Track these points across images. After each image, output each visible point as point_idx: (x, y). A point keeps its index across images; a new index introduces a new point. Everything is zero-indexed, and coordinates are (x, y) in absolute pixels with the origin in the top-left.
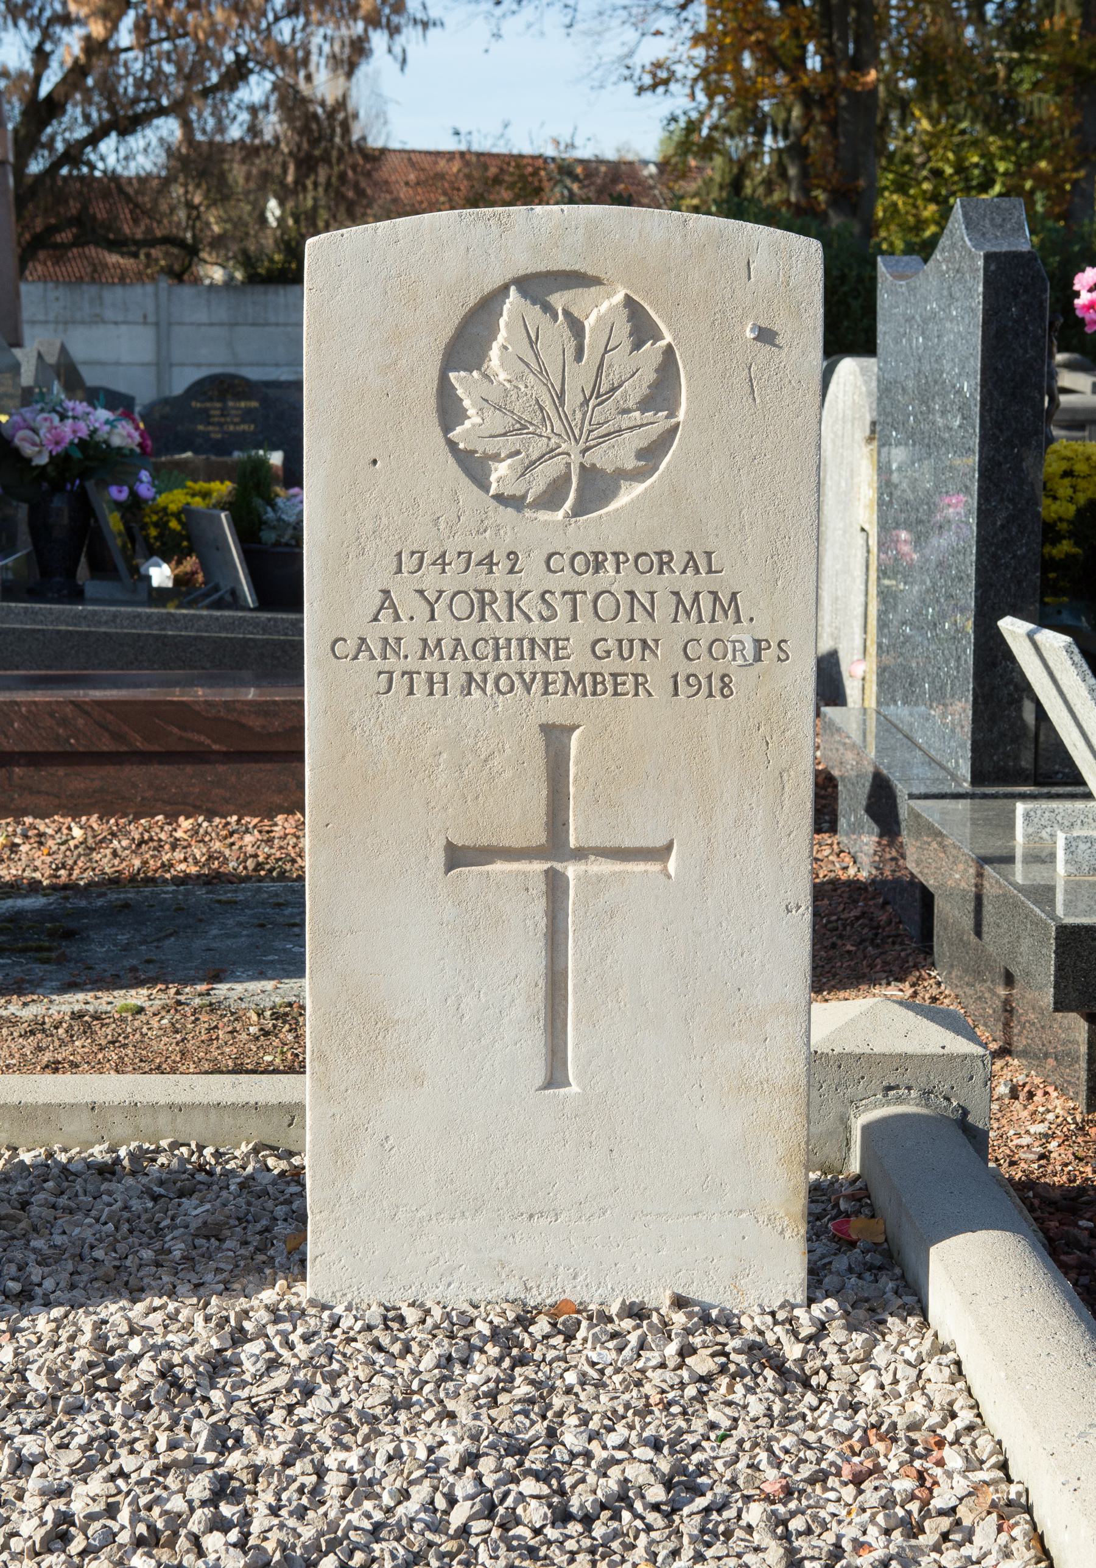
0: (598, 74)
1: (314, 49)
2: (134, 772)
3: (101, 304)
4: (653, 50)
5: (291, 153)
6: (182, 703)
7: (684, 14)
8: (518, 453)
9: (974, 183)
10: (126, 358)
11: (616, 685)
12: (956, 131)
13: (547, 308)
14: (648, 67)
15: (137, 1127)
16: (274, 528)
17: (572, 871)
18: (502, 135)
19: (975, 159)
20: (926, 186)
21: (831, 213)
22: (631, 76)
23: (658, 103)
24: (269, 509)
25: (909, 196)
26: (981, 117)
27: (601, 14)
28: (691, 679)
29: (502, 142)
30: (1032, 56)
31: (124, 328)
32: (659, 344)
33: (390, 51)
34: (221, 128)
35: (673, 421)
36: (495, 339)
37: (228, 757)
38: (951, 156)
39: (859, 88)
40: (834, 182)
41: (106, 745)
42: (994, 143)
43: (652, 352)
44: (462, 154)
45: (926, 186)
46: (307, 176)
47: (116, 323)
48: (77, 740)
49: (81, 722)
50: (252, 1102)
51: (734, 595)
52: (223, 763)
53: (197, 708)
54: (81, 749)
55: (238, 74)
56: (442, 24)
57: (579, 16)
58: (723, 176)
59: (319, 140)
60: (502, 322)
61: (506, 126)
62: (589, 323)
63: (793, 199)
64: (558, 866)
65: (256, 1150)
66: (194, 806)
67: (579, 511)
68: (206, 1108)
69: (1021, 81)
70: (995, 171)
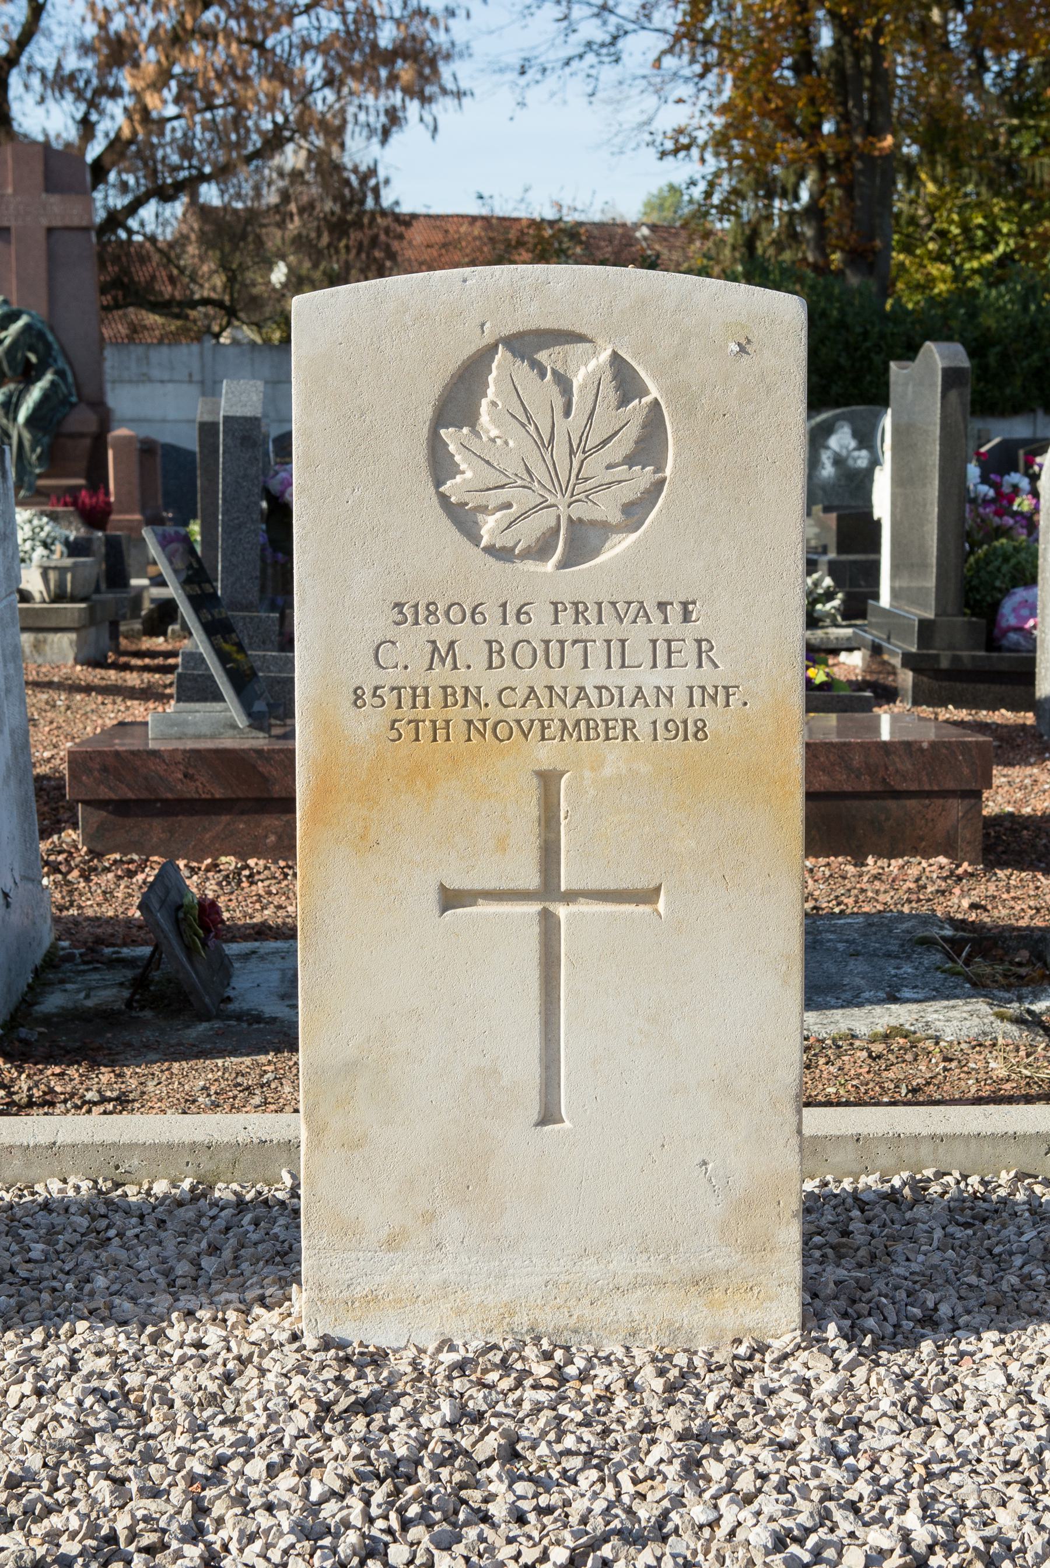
0: (618, 140)
1: (350, 118)
3: (148, 364)
4: (672, 117)
5: (749, 222)
7: (702, 84)
8: (509, 506)
9: (978, 244)
10: (172, 415)
11: (607, 729)
12: (960, 194)
13: (535, 365)
14: (670, 134)
15: (900, 1157)
17: (562, 911)
18: (522, 200)
19: (980, 220)
20: (931, 246)
21: (848, 272)
22: (654, 142)
23: (677, 168)
25: (915, 256)
26: (986, 181)
27: (621, 83)
29: (523, 206)
30: (1031, 122)
31: (170, 387)
32: (644, 400)
33: (421, 120)
34: (258, 194)
39: (876, 153)
40: (852, 242)
42: (998, 205)
44: (484, 218)
45: (931, 246)
46: (339, 240)
47: (162, 382)
50: (1011, 1132)
51: (452, 644)
55: (275, 141)
56: (472, 94)
57: (601, 86)
58: (735, 239)
59: (351, 203)
60: (491, 379)
61: (526, 190)
62: (577, 382)
63: (811, 258)
64: (552, 907)
65: (1020, 1177)
67: (563, 565)
68: (966, 1139)
69: (1020, 147)
70: (999, 231)
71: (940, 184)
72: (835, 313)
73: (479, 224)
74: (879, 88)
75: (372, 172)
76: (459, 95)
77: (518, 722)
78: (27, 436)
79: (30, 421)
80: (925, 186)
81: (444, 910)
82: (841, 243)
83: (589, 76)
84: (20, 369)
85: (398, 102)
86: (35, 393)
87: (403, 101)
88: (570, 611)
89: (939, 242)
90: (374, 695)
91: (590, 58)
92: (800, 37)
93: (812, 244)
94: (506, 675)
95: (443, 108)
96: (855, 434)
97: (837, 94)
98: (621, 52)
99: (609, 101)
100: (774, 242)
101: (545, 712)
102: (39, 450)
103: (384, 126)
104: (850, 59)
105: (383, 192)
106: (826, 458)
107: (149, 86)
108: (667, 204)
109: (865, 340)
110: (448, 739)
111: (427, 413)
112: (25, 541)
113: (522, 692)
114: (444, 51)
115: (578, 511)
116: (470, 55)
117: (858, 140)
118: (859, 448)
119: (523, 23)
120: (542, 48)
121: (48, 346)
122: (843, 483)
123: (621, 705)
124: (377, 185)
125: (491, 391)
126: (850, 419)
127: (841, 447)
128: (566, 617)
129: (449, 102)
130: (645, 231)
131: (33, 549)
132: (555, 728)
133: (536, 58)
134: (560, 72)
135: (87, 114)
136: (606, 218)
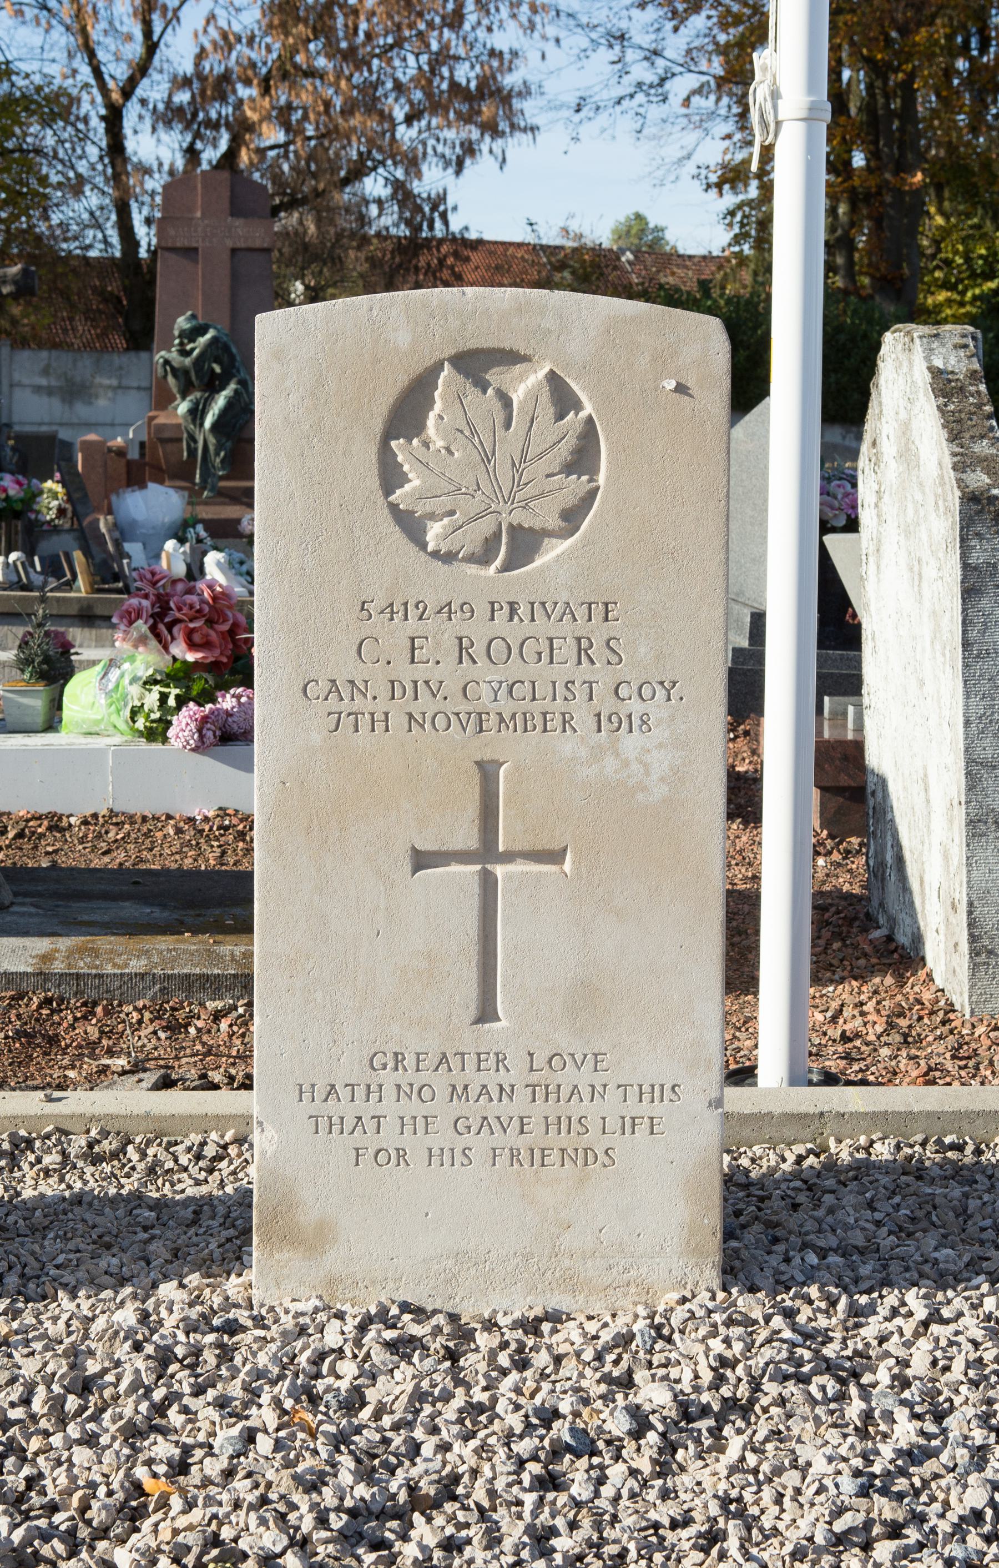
0: (659, 173)
1: (430, 150)
8: (452, 513)
9: (979, 271)
17: (500, 871)
26: (990, 214)
27: (664, 121)
33: (491, 151)
35: (593, 485)
38: (960, 248)
60: (437, 394)
71: (946, 216)
74: (910, 128)
75: (442, 198)
78: (212, 440)
79: (215, 427)
81: (414, 872)
82: (871, 271)
84: (206, 380)
86: (220, 401)
88: (506, 608)
89: (946, 270)
93: (842, 272)
95: (516, 146)
98: (667, 92)
99: (654, 137)
102: (222, 454)
103: (458, 157)
104: (881, 101)
105: (451, 217)
108: (633, 231)
111: (377, 426)
114: (516, 89)
115: (519, 517)
117: (888, 176)
119: (579, 65)
121: (232, 357)
125: (438, 407)
129: (526, 138)
130: (629, 255)
133: (591, 97)
134: (611, 110)
135: (192, 144)
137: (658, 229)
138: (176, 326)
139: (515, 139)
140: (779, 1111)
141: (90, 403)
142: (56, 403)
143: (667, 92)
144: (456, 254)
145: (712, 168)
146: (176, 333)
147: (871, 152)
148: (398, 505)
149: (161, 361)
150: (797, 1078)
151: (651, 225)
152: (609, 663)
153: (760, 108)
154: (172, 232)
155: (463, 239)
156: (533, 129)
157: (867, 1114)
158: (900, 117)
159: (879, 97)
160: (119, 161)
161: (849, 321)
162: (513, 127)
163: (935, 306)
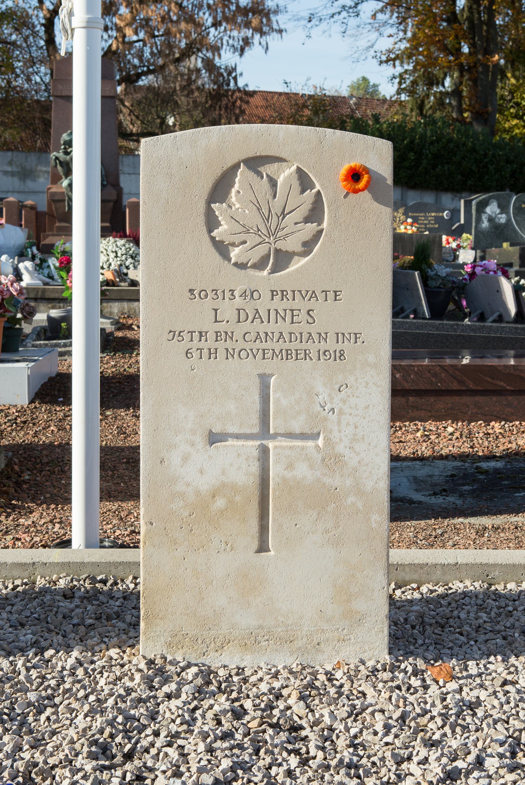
1: (225, 42)
2: (467, 399)
6: (493, 366)
8: (245, 242)
11: (297, 354)
16: (434, 279)
17: (271, 445)
18: (306, 85)
20: (512, 110)
22: (376, 56)
24: (429, 270)
25: (504, 115)
27: (358, 27)
28: (327, 353)
29: (306, 88)
33: (260, 44)
36: (233, 186)
37: (514, 393)
41: (455, 386)
43: (309, 194)
44: (287, 94)
48: (441, 384)
49: (443, 375)
52: (511, 395)
53: (500, 368)
54: (443, 388)
56: (286, 31)
57: (349, 27)
60: (237, 180)
62: (280, 181)
64: (264, 442)
66: (496, 416)
67: (274, 271)
72: (470, 144)
73: (283, 97)
74: (491, 31)
75: (234, 69)
76: (280, 31)
77: (252, 350)
80: (509, 80)
82: (471, 108)
83: (343, 23)
85: (250, 35)
87: (253, 34)
90: (179, 335)
91: (344, 14)
92: (451, 5)
94: (246, 326)
95: (272, 39)
96: (499, 206)
97: (469, 34)
98: (359, 11)
99: (352, 36)
100: (431, 107)
101: (264, 345)
103: (241, 46)
106: (484, 217)
107: (127, 25)
109: (485, 158)
110: (216, 358)
112: (122, 255)
113: (253, 335)
114: (273, 9)
115: (280, 245)
116: (287, 12)
117: (480, 57)
118: (501, 213)
120: (320, 9)
122: (493, 231)
123: (301, 342)
124: (236, 76)
126: (497, 198)
127: (492, 212)
128: (277, 298)
129: (275, 35)
131: (126, 259)
132: (269, 355)
133: (317, 13)
134: (328, 21)
136: (336, 94)
137: (375, 86)
138: (62, 139)
139: (271, 37)
140: (11, 561)
141: (35, 181)
142: (16, 180)
143: (359, 11)
144: (241, 99)
145: (384, 53)
146: (62, 142)
147: (471, 44)
148: (215, 238)
149: (54, 157)
150: (89, 545)
151: (371, 84)
152: (308, 322)
153: (62, 21)
154: (60, 87)
155: (245, 90)
156: (280, 31)
157: (58, 563)
158: (487, 24)
159: (475, 14)
160: (51, 48)
161: (455, 136)
162: (272, 29)
163: (510, 128)
